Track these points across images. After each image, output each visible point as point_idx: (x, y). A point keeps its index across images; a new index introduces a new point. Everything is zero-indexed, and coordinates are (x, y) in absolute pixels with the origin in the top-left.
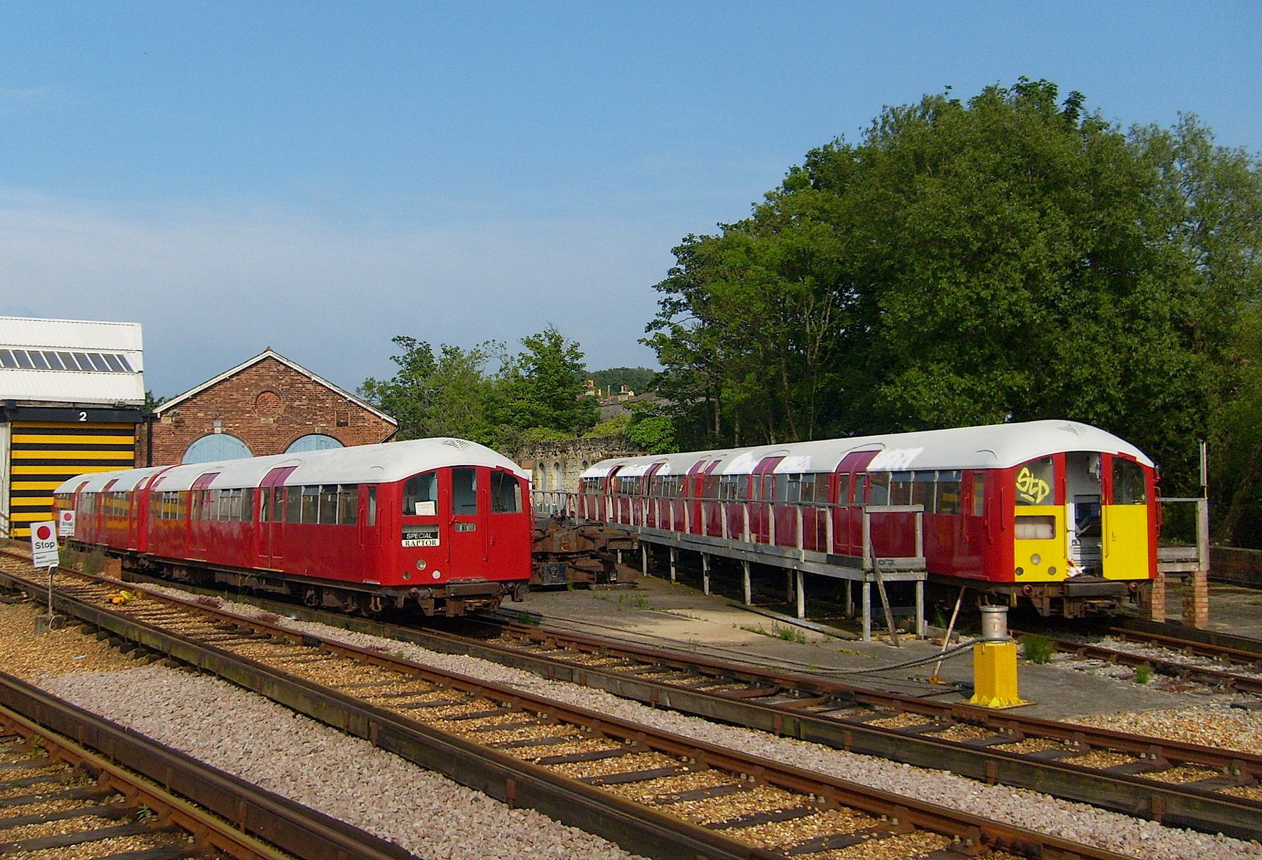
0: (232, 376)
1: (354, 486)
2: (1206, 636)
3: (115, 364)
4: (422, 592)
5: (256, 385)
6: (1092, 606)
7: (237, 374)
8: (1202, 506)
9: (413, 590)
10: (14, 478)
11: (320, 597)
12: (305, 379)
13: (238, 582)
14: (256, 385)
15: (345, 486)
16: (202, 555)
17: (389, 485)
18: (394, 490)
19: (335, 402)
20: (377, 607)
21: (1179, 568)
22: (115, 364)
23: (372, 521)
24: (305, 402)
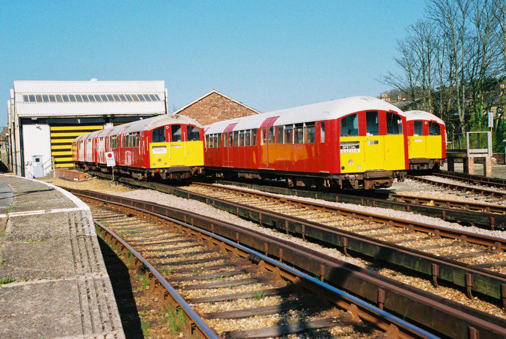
0: (199, 101)
1: (313, 123)
2: (491, 180)
3: (154, 98)
4: (351, 176)
5: (209, 104)
6: (378, 183)
7: (201, 100)
8: (490, 134)
9: (347, 176)
10: (53, 151)
11: (295, 183)
12: (229, 101)
13: (249, 176)
14: (209, 104)
15: (307, 124)
16: (230, 164)
17: (332, 121)
18: (336, 122)
19: (241, 109)
20: (327, 185)
21: (480, 156)
22: (154, 98)
23: (323, 140)
24: (229, 110)
